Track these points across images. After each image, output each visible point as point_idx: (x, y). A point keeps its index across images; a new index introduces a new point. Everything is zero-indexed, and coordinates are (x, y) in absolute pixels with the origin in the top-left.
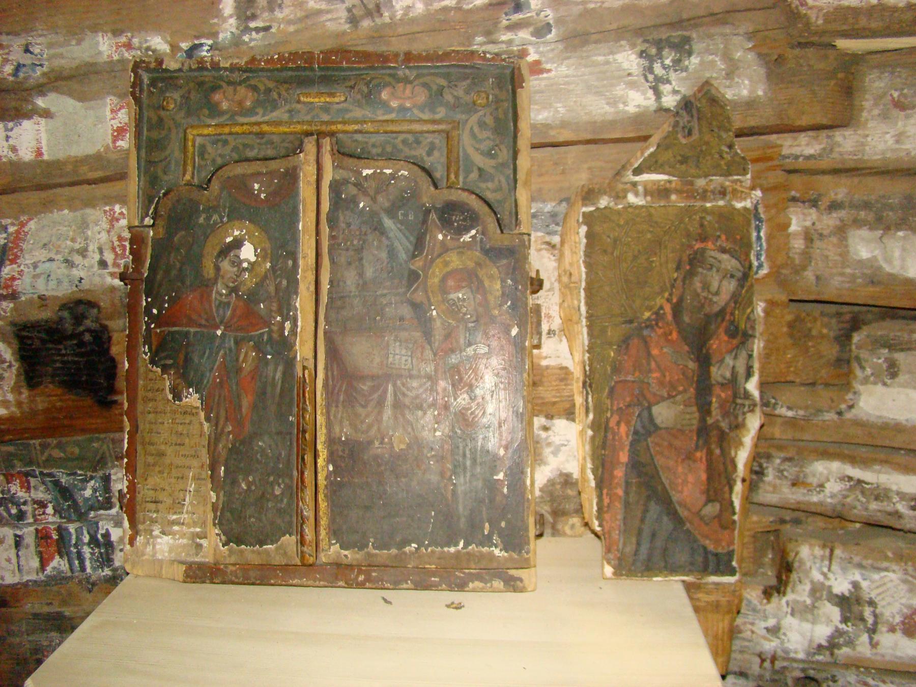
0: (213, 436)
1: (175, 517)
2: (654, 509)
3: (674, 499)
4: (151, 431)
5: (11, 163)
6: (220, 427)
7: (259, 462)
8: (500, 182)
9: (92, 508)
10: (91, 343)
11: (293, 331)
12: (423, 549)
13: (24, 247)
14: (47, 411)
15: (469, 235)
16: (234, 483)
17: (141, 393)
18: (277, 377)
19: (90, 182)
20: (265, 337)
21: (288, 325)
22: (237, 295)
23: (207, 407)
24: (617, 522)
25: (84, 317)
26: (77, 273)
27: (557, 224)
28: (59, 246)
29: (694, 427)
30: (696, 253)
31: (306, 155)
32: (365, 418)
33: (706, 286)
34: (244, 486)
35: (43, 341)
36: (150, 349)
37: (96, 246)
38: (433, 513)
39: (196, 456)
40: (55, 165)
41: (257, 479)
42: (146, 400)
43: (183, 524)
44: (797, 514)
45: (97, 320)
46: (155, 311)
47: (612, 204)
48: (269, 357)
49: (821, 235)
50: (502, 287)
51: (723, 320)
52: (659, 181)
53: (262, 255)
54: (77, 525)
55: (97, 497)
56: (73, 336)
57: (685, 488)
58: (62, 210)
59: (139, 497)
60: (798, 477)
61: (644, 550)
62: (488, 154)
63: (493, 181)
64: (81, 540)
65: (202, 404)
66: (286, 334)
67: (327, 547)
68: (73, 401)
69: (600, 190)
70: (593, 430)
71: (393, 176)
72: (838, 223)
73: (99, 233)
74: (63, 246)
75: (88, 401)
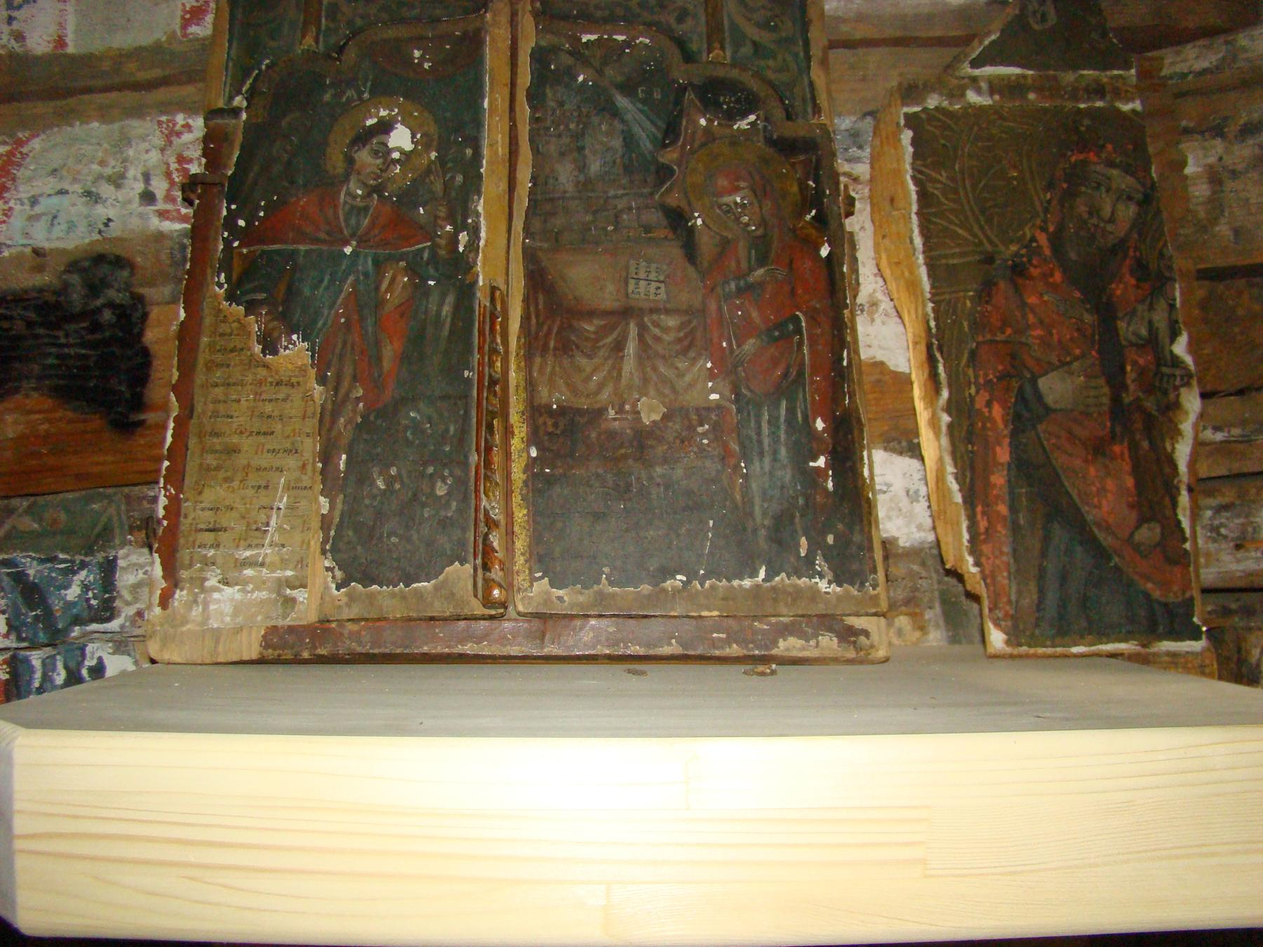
0: (329, 407)
1: (248, 553)
2: (1059, 534)
3: (1089, 518)
4: (216, 414)
5: (12, 56)
6: (342, 391)
7: (409, 443)
8: (784, 60)
9: (78, 621)
10: (112, 326)
11: (473, 245)
12: (697, 584)
13: (19, 174)
14: (21, 439)
15: (746, 122)
16: (364, 480)
17: (203, 357)
18: (444, 313)
19: (137, 87)
20: (426, 256)
21: (463, 237)
22: (381, 196)
23: (322, 361)
24: (1005, 558)
25: (105, 283)
26: (101, 211)
27: (860, 147)
28: (79, 172)
29: (1106, 408)
30: (1074, 166)
31: (495, 15)
32: (592, 374)
33: (1094, 211)
34: (381, 484)
35: (30, 324)
36: (228, 279)
37: (141, 169)
38: (711, 522)
39: (293, 451)
40: (86, 61)
41: (404, 473)
42: (211, 366)
43: (262, 565)
44: (1247, 598)
45: (128, 286)
46: (242, 223)
47: (945, 104)
48: (432, 283)
49: (1233, 172)
50: (801, 190)
51: (1125, 256)
52: (1009, 76)
53: (424, 143)
54: (48, 651)
55: (88, 600)
56: (84, 315)
57: (1104, 501)
58: (87, 123)
59: (185, 524)
60: (1244, 532)
61: (1052, 598)
62: (764, 25)
63: (774, 58)
64: (52, 681)
65: (313, 356)
66: (461, 249)
67: (526, 585)
68: (70, 421)
69: (925, 85)
70: (950, 415)
71: (627, 44)
72: (1257, 151)
73: (147, 151)
74: (86, 171)
75: (96, 422)
